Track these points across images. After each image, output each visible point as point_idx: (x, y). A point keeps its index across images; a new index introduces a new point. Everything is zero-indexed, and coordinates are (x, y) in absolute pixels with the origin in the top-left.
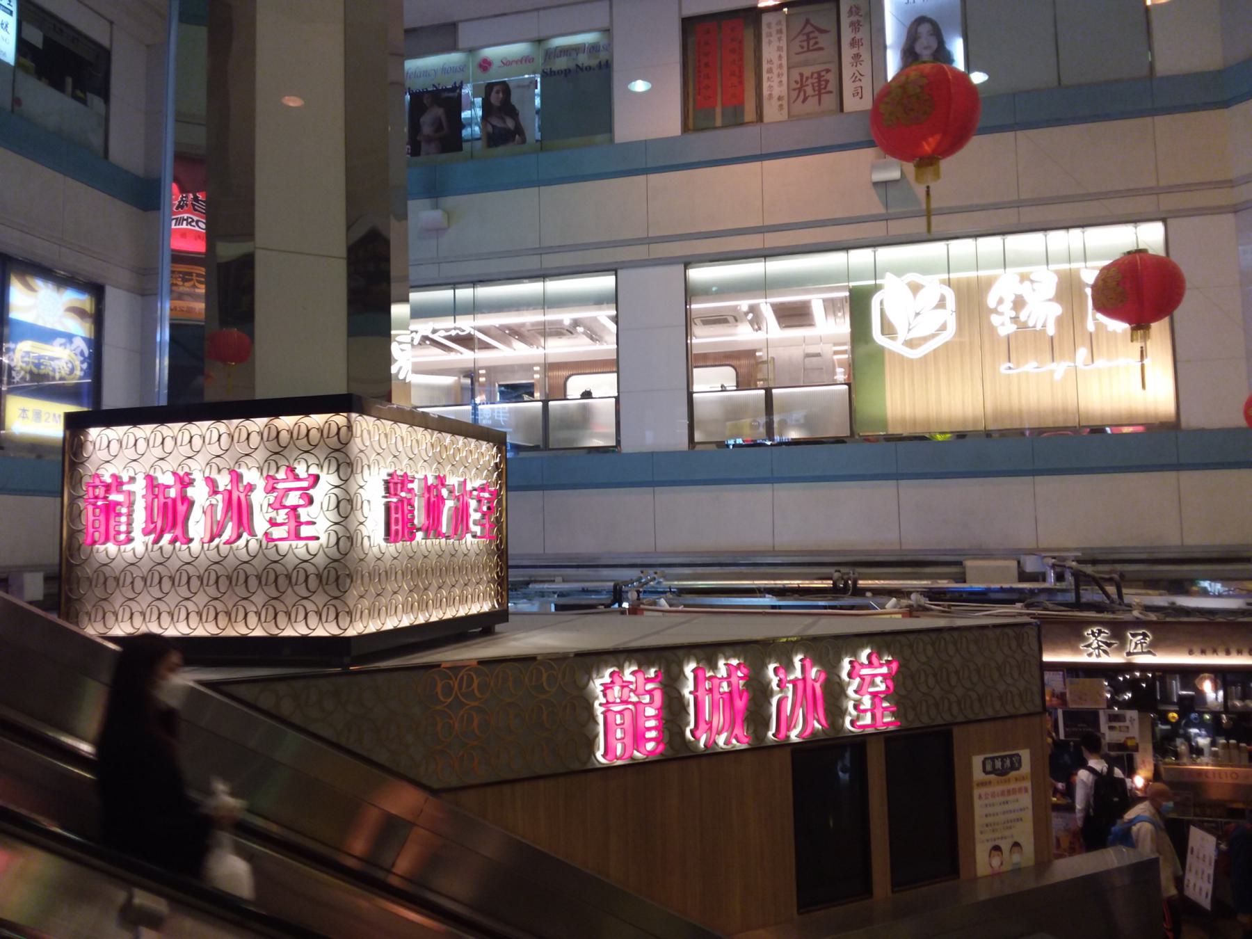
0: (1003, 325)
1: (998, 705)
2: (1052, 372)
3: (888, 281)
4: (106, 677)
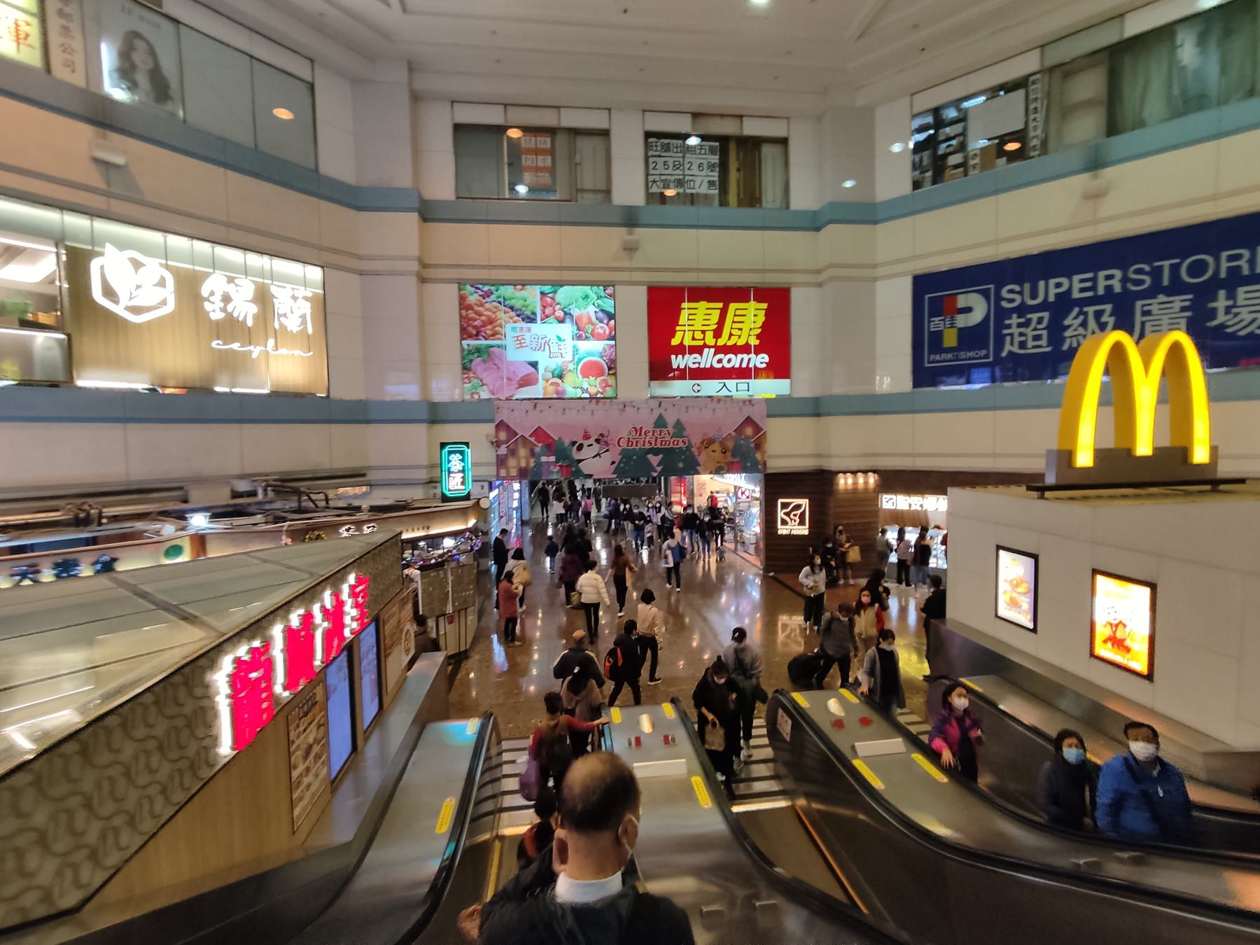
2: (251, 352)
3: (109, 249)
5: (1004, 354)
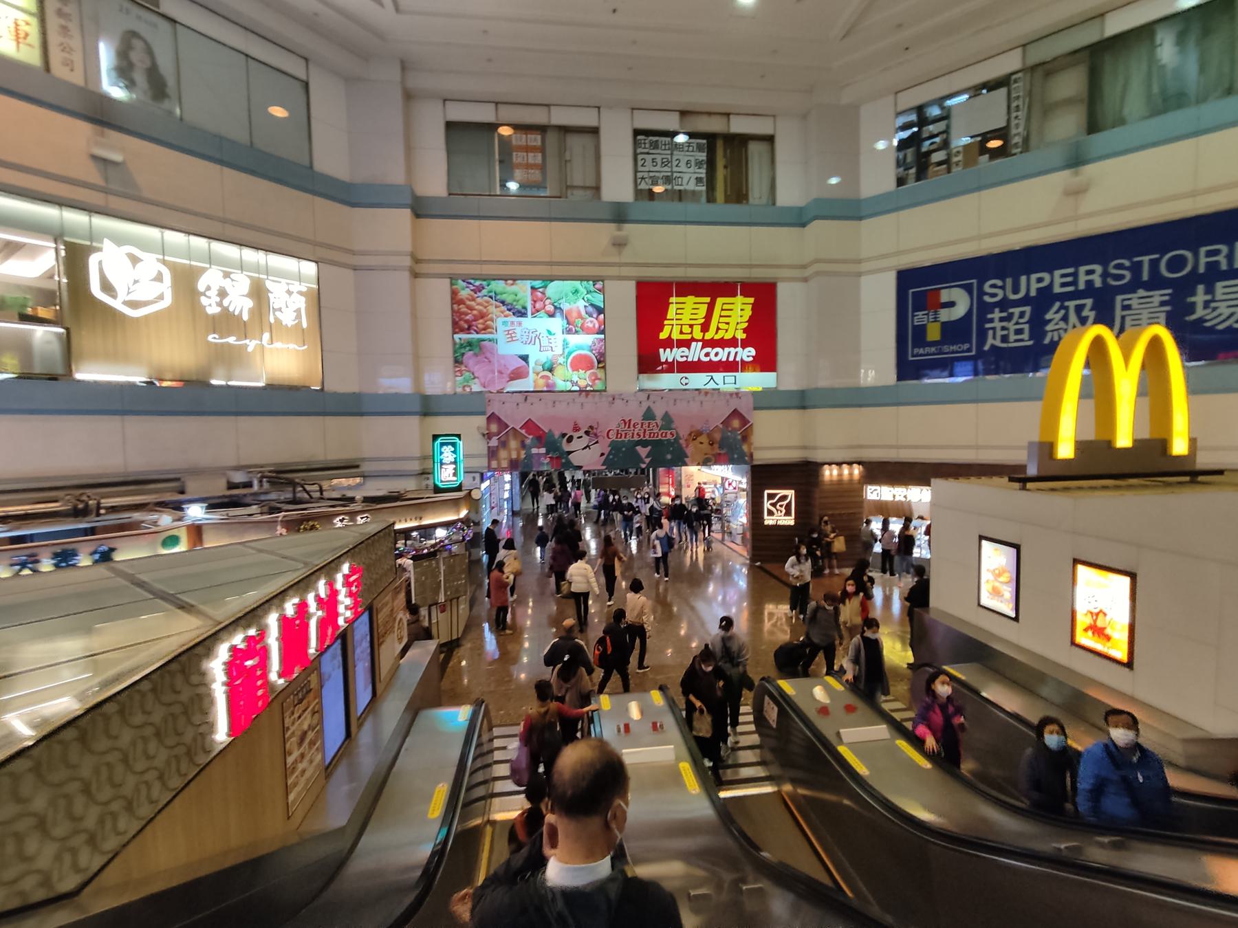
2: (247, 346)
3: (107, 244)
5: (986, 348)
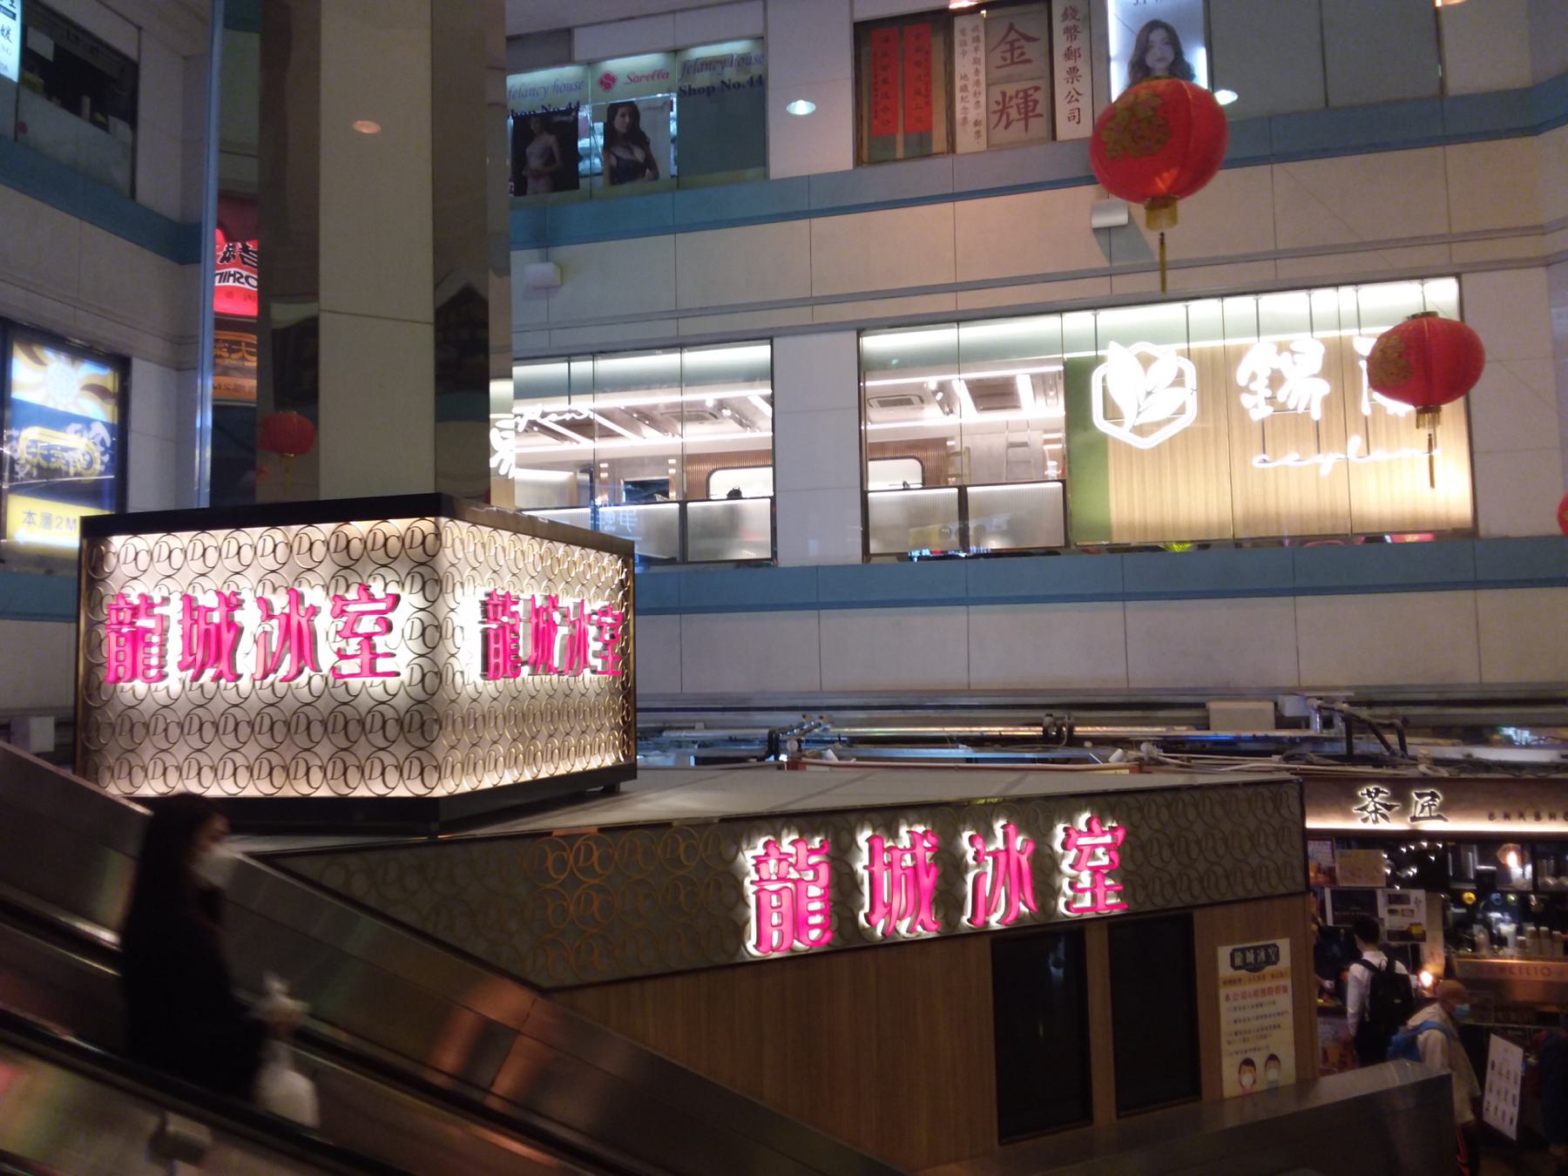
0: (1257, 407)
1: (1250, 883)
2: (1317, 466)
3: (1113, 352)
4: (133, 848)
